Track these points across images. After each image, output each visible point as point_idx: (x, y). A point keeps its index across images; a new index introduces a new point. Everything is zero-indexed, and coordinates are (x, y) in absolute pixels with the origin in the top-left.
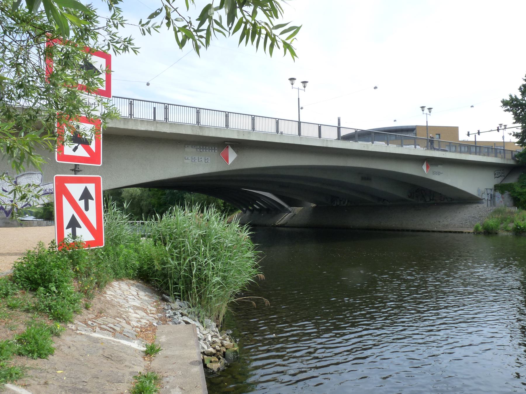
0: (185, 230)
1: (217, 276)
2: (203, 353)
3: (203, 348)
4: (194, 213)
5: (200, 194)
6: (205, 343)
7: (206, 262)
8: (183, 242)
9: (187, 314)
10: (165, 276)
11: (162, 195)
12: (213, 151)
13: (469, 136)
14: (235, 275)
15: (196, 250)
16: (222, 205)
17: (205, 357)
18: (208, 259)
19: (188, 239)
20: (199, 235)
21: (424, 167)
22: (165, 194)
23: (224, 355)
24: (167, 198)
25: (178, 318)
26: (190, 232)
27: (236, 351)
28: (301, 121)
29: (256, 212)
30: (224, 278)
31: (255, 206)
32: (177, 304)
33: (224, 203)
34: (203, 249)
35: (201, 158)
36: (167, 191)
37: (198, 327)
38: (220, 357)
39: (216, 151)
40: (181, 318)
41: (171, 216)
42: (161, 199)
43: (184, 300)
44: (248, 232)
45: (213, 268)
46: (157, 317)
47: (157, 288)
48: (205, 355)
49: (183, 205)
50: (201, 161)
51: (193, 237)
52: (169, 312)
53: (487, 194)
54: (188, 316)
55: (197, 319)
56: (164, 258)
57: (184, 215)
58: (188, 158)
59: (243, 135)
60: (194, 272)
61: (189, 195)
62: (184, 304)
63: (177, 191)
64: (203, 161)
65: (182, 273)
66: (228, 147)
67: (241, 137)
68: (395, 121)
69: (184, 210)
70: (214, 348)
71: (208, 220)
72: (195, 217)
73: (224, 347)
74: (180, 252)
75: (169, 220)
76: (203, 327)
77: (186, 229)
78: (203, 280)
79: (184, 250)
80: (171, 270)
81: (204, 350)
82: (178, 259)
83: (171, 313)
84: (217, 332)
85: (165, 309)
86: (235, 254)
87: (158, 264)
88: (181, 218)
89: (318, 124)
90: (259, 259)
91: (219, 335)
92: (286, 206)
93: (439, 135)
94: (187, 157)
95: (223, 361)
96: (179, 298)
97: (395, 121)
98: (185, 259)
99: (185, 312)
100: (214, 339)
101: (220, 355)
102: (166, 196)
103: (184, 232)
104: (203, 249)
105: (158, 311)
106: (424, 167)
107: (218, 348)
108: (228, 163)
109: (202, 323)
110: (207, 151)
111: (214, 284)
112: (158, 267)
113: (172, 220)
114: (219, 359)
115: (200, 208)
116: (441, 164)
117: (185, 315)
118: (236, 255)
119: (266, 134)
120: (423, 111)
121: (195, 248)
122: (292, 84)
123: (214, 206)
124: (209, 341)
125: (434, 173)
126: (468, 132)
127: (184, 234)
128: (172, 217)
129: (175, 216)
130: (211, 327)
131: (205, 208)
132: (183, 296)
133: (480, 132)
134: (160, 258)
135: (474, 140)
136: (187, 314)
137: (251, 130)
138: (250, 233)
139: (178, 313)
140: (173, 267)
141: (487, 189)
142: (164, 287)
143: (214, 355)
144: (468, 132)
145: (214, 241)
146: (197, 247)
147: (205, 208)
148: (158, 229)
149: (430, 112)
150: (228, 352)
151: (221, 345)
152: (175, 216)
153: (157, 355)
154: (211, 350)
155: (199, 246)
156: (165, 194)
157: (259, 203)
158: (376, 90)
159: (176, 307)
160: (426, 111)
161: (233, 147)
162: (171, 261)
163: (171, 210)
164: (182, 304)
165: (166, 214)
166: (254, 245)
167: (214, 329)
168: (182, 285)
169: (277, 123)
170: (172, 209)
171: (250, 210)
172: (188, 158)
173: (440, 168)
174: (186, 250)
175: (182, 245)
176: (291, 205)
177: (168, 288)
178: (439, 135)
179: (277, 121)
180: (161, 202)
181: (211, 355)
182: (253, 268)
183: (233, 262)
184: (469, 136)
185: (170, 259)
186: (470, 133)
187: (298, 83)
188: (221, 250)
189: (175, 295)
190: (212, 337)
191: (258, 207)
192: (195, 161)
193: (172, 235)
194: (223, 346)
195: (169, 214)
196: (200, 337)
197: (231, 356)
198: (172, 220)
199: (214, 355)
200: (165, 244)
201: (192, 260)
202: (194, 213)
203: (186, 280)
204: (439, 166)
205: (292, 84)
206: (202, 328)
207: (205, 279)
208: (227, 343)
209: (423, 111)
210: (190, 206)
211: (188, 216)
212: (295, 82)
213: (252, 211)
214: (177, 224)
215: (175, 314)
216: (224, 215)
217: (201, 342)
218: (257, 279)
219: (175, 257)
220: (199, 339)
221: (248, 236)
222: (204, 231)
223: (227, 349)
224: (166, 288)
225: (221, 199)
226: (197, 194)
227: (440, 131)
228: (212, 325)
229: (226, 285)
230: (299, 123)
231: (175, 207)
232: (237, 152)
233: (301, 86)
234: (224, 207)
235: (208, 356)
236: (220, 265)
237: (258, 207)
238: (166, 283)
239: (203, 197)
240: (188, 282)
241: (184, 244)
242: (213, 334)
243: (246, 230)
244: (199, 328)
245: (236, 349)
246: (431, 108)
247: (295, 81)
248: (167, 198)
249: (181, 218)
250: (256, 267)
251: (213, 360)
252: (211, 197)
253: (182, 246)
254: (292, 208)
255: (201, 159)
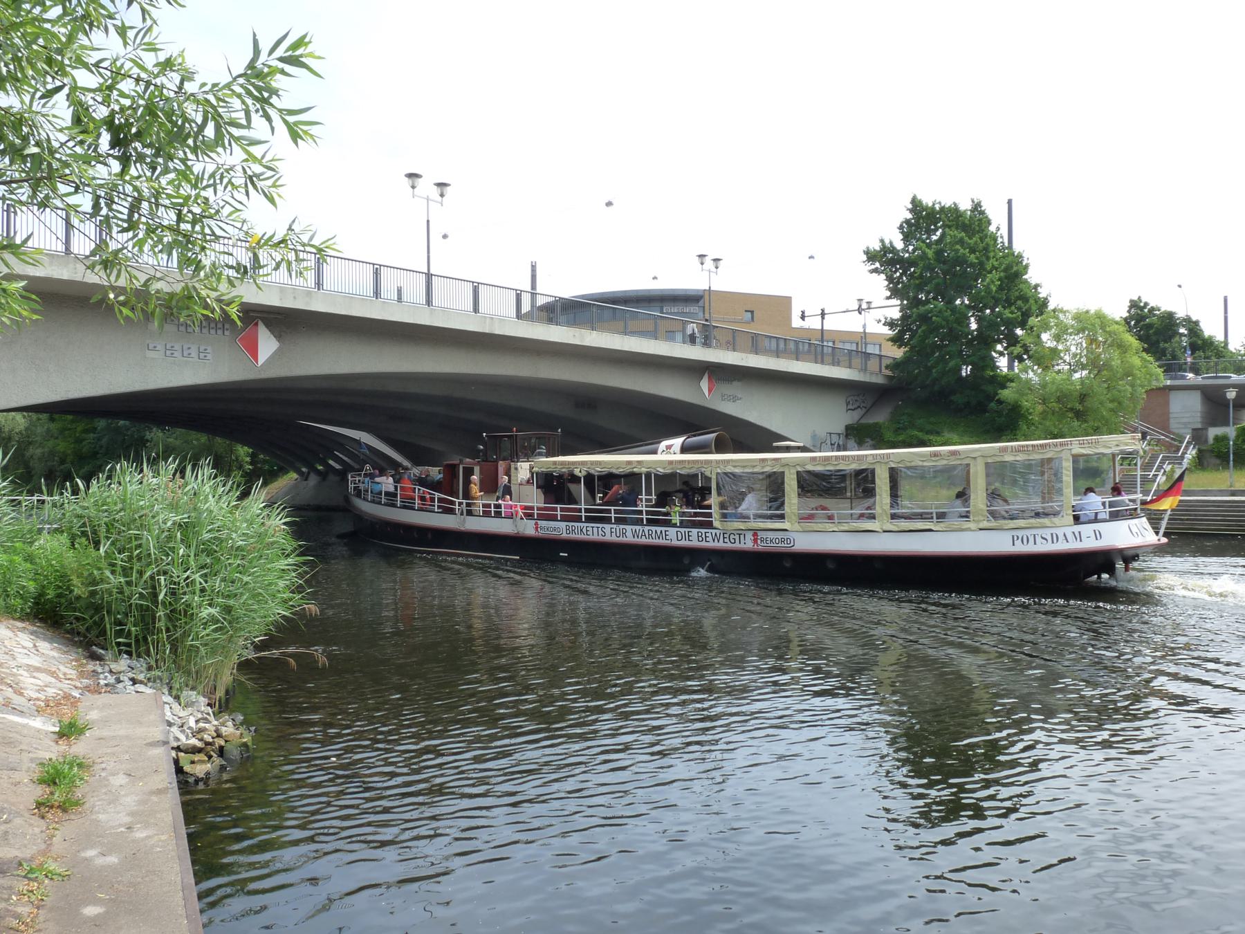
0: (142, 513)
1: (210, 605)
2: (178, 749)
3: (177, 739)
4: (164, 479)
5: (191, 432)
6: (183, 732)
7: (188, 578)
8: (137, 537)
9: (145, 681)
10: (97, 609)
11: (86, 431)
12: (220, 332)
13: (804, 320)
14: (248, 605)
15: (168, 555)
16: (248, 459)
17: (182, 754)
18: (193, 573)
19: (149, 531)
20: (174, 523)
21: (704, 384)
22: (94, 430)
23: (221, 752)
24: (99, 439)
25: (125, 687)
26: (153, 517)
27: (245, 745)
28: (432, 271)
29: (332, 478)
30: (228, 610)
31: (331, 462)
32: (123, 663)
33: (253, 456)
34: (181, 552)
35: (189, 348)
36: (101, 423)
37: (169, 704)
38: (212, 753)
39: (227, 333)
40: (132, 688)
41: (110, 484)
42: (84, 443)
43: (139, 656)
44: (286, 517)
45: (203, 590)
46: (79, 685)
47: (79, 633)
48: (181, 751)
49: (138, 460)
50: (189, 354)
51: (160, 527)
52: (106, 677)
53: (831, 444)
54: (146, 685)
55: (166, 691)
56: (95, 572)
57: (141, 483)
58: (155, 347)
59: (295, 298)
60: (161, 597)
61: (160, 434)
62: (140, 664)
63: (127, 423)
64: (194, 354)
65: (132, 601)
66: (256, 324)
67: (289, 303)
68: (655, 278)
69: (142, 471)
70: (201, 740)
71: (195, 494)
72: (167, 486)
73: (222, 737)
74: (130, 558)
75: (106, 494)
76: (180, 705)
77: (146, 511)
78: (179, 615)
79: (138, 555)
80: (111, 595)
81: (179, 743)
82: (126, 572)
83: (111, 679)
84: (208, 714)
85: (97, 673)
86: (250, 563)
87: (79, 585)
88: (134, 487)
89: (473, 282)
90: (306, 573)
91: (212, 718)
92: (406, 463)
93: (752, 312)
94: (153, 345)
95: (218, 761)
96: (128, 649)
97: (655, 278)
98: (141, 573)
99: (141, 677)
100: (201, 725)
101: (213, 750)
102: (95, 435)
103: (140, 517)
104: (181, 552)
105: (82, 675)
106: (704, 384)
107: (208, 738)
108: (256, 360)
109: (177, 698)
110: (204, 331)
111: (205, 621)
112: (79, 590)
113: (113, 492)
114: (210, 757)
115: (178, 465)
116: (739, 380)
117: (141, 682)
118: (255, 563)
119: (350, 298)
120: (702, 264)
121: (165, 551)
122: (413, 187)
123: (209, 464)
124: (190, 728)
125: (724, 398)
126: (803, 312)
127: (140, 522)
128: (113, 486)
129: (120, 483)
130: (196, 704)
131: (189, 468)
132: (135, 647)
133: (826, 312)
134: (86, 574)
135: (820, 328)
136: (145, 681)
137: (313, 286)
138: (288, 519)
139: (126, 679)
140: (115, 590)
141: (830, 434)
142: (94, 632)
143: (200, 750)
144: (803, 312)
145: (207, 536)
146: (170, 548)
147: (189, 468)
148: (79, 511)
149: (717, 268)
150: (228, 747)
151: (215, 735)
152: (120, 483)
153: (82, 737)
154: (194, 742)
155: (174, 547)
156: (94, 430)
157: (341, 456)
158: (610, 208)
159: (123, 669)
160: (709, 264)
161: (269, 325)
162: (111, 577)
163: (110, 470)
164: (134, 663)
165: (98, 478)
166: (295, 544)
167: (203, 708)
168: (135, 626)
169: (377, 273)
170: (113, 469)
171: (319, 473)
172: (155, 347)
173: (735, 388)
174: (145, 553)
175: (135, 543)
176: (417, 462)
177: (103, 633)
178: (752, 312)
179: (377, 269)
180: (84, 450)
181: (195, 750)
182: (293, 592)
183: (246, 579)
184: (804, 320)
185: (108, 573)
186: (806, 315)
187: (426, 186)
188: (222, 555)
189: (119, 644)
190: (197, 722)
191: (338, 467)
192: (172, 354)
193: (113, 525)
194: (219, 736)
195: (107, 480)
196: (172, 721)
197: (234, 753)
198: (113, 492)
199: (200, 750)
200: (97, 545)
201: (159, 573)
202: (164, 479)
203: (143, 616)
204: (736, 383)
205: (413, 187)
206: (175, 706)
207: (186, 612)
208: (228, 729)
209: (702, 264)
210: (153, 462)
211: (149, 485)
212: (419, 182)
213: (323, 475)
214: (124, 501)
215: (119, 681)
216: (230, 483)
217: (175, 729)
218: (302, 614)
219: (119, 569)
220: (170, 724)
221: (285, 527)
222: (186, 516)
223: (226, 741)
224: (100, 633)
225: (244, 443)
226: (179, 431)
227: (753, 306)
228: (197, 701)
229: (230, 623)
230: (429, 276)
231: (121, 466)
232: (279, 337)
233: (435, 192)
234: (251, 464)
235: (186, 752)
236: (217, 583)
237: (338, 467)
238: (100, 624)
239: (197, 440)
240: (146, 618)
241: (139, 542)
242: (200, 716)
243: (279, 514)
244: (171, 708)
245: (245, 740)
246: (719, 260)
247: (420, 180)
248: (99, 439)
249: (134, 487)
250: (299, 590)
251: (196, 759)
252: (219, 440)
253: (136, 546)
254: (420, 468)
255: (189, 351)
